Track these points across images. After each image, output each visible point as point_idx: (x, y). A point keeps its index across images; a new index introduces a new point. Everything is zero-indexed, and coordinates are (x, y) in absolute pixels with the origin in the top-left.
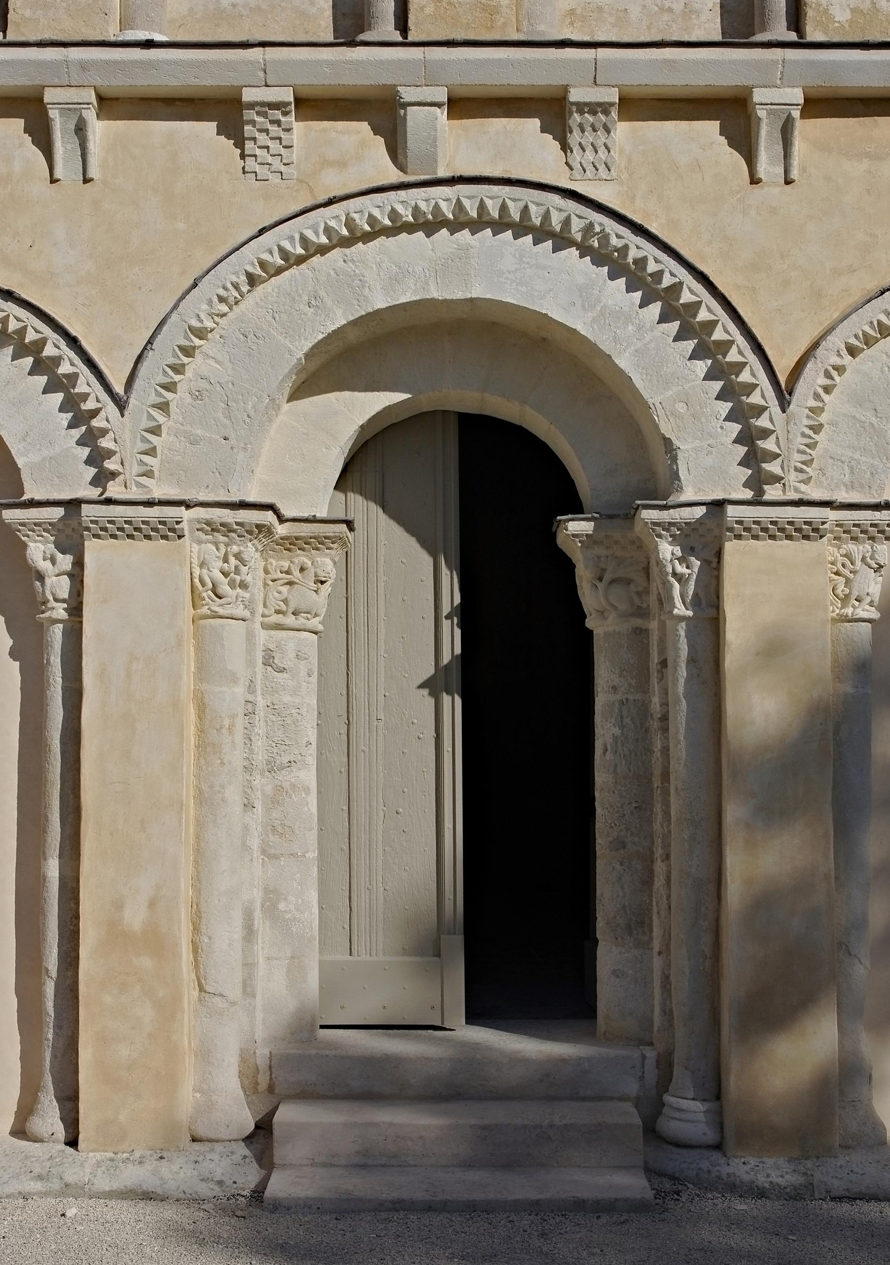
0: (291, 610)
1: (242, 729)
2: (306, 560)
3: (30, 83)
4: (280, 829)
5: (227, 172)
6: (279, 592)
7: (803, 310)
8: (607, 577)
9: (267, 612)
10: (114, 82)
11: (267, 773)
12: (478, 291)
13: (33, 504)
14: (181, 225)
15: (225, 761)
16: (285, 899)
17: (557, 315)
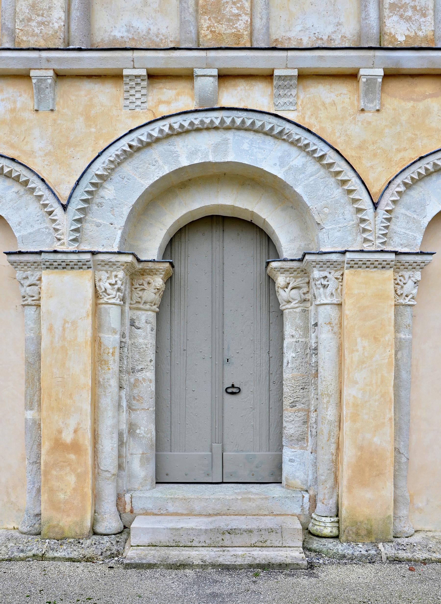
0: (143, 302)
1: (118, 354)
2: (150, 279)
3: (24, 68)
4: (137, 398)
5: (115, 106)
6: (138, 294)
7: (383, 167)
8: (290, 286)
9: (132, 302)
11: (131, 373)
12: (231, 158)
13: (285, 260)
15: (110, 368)
16: (140, 429)
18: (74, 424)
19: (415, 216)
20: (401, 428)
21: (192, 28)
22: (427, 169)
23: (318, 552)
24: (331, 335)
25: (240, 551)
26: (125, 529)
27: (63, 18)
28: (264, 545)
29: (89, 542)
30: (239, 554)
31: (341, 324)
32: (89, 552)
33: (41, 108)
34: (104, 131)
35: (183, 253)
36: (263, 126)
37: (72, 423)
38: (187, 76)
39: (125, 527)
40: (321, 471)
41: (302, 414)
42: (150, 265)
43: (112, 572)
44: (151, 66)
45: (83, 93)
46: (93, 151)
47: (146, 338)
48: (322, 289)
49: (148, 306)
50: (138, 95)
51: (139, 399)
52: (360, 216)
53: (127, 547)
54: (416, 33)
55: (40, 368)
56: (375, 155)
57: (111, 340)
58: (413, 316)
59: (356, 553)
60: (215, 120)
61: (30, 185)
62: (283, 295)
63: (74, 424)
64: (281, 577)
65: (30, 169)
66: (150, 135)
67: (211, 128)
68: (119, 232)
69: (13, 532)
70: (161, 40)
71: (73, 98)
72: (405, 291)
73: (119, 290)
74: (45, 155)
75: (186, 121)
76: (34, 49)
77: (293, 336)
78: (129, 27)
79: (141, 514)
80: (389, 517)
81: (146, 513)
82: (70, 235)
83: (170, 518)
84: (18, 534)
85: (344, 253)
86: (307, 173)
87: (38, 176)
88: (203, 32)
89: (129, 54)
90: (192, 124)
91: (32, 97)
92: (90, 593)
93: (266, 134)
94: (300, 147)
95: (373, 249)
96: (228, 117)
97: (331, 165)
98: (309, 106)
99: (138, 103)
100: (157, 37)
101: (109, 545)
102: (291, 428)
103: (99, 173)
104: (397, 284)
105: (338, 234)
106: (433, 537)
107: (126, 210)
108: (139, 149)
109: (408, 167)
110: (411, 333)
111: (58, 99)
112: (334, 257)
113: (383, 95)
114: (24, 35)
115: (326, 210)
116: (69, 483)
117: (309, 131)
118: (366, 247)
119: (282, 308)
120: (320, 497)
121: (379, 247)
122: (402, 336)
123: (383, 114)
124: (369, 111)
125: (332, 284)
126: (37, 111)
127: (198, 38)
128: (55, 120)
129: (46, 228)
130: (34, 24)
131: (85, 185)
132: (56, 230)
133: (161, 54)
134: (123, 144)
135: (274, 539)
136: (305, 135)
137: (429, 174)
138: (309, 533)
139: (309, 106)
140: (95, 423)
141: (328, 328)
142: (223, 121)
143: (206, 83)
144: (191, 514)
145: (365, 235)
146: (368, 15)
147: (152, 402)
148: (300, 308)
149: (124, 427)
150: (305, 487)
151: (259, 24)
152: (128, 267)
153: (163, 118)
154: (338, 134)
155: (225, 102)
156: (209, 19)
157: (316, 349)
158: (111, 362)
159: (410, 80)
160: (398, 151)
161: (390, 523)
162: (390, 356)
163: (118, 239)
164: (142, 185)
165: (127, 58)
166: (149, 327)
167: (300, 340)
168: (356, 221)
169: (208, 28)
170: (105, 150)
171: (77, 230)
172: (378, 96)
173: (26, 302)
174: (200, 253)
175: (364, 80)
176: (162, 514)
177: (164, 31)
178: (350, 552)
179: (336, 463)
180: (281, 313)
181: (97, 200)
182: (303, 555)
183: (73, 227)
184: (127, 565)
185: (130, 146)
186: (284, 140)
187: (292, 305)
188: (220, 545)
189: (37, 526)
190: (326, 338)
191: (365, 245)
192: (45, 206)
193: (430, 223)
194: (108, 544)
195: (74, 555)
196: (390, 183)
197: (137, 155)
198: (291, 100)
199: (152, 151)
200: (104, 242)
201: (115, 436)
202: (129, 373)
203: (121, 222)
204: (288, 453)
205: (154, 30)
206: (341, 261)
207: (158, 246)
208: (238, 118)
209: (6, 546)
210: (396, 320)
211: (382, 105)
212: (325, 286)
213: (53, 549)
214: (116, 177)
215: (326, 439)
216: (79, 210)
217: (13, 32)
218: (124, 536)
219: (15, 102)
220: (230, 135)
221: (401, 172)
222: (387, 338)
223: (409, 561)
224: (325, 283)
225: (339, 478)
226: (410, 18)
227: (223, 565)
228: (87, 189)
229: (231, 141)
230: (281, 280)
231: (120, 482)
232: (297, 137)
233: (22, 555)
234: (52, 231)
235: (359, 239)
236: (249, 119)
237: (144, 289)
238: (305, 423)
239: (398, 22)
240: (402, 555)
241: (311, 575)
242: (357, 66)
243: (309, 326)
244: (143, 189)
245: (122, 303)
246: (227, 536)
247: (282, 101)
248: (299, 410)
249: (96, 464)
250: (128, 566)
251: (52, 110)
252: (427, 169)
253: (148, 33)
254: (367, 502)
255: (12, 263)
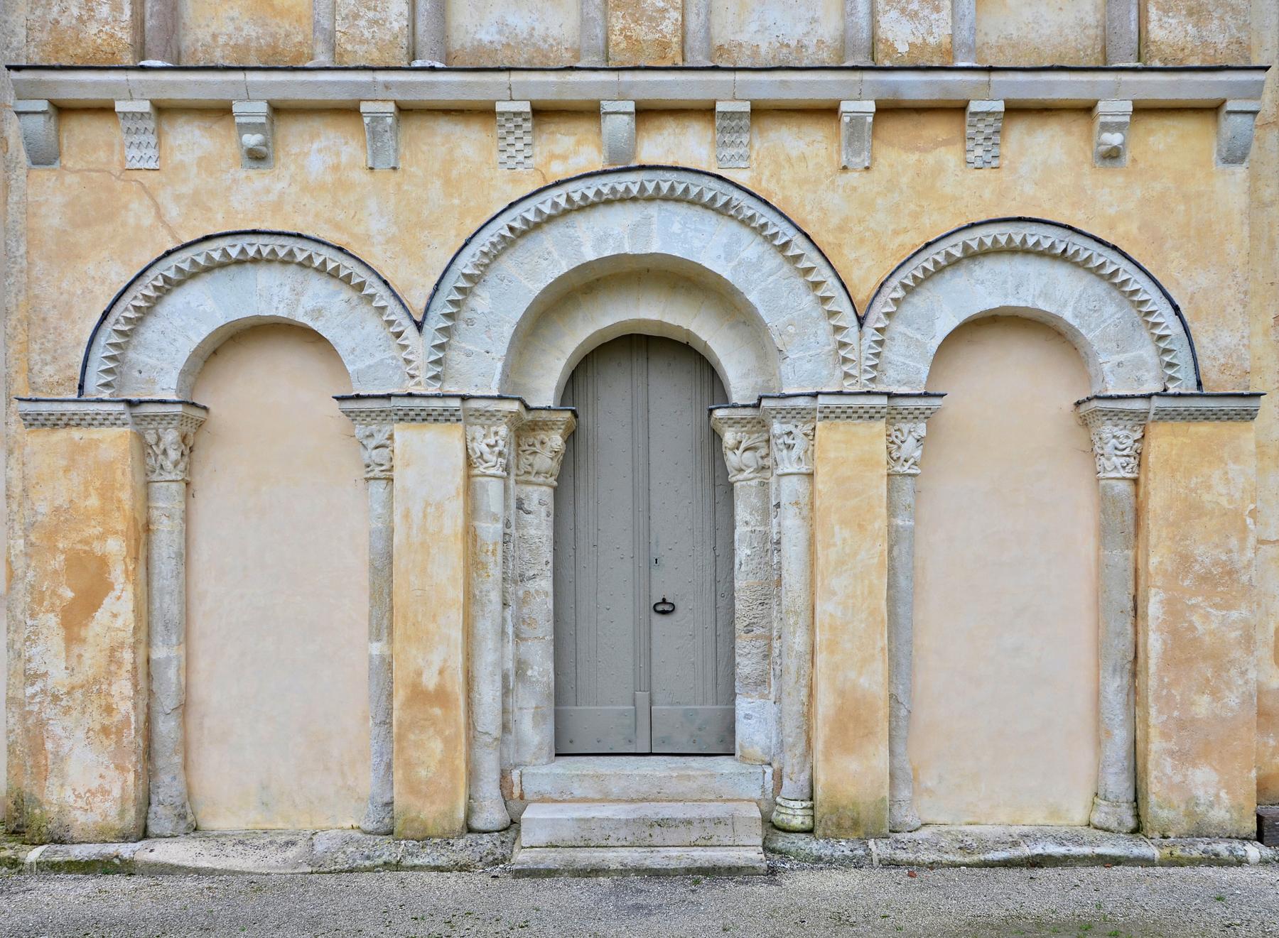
8: (742, 447)
10: (408, 98)
12: (655, 247)
13: (735, 406)
14: (456, 201)
17: (706, 265)
18: (436, 660)
19: (919, 336)
20: (899, 660)
21: (598, 30)
22: (936, 263)
23: (784, 854)
24: (798, 522)
25: (674, 852)
26: (513, 825)
27: (406, 13)
28: (709, 843)
29: (462, 842)
30: (673, 856)
31: (812, 504)
32: (463, 858)
33: (378, 165)
34: (472, 204)
35: (590, 395)
36: (700, 194)
37: (436, 659)
38: (589, 112)
39: (512, 822)
40: (787, 731)
41: (761, 642)
42: (544, 414)
43: (497, 882)
44: (538, 96)
45: (438, 140)
46: (457, 235)
47: (539, 527)
48: (785, 451)
49: (541, 479)
50: (519, 145)
51: (531, 622)
52: (838, 338)
53: (516, 850)
54: (924, 40)
55: (391, 575)
56: (862, 241)
57: (490, 530)
58: (917, 492)
59: (836, 855)
60: (631, 186)
61: (367, 291)
62: (733, 459)
63: (436, 660)
64: (730, 885)
65: (367, 265)
66: (539, 212)
67: (627, 199)
68: (499, 365)
69: (352, 832)
70: (551, 46)
71: (425, 148)
72: (904, 453)
73: (500, 454)
74: (387, 242)
75: (589, 189)
76: (365, 69)
77: (747, 523)
78: (502, 25)
79: (535, 801)
80: (883, 799)
81: (543, 799)
82: (429, 370)
83: (576, 805)
84: (358, 835)
85: (815, 395)
86: (764, 270)
87: (379, 277)
88: (614, 37)
89: (503, 77)
90: (598, 193)
91: (364, 147)
92: (469, 907)
93: (705, 206)
94: (754, 228)
95: (856, 389)
96: (650, 181)
97: (797, 258)
98: (767, 161)
99: (520, 157)
100: (545, 41)
101: (491, 844)
102: (746, 666)
103: (467, 271)
104: (892, 442)
105: (809, 366)
106: (948, 832)
107: (508, 331)
108: (523, 234)
109: (909, 259)
110: (913, 517)
111: (402, 150)
112: (801, 402)
113: (875, 143)
114: (348, 41)
115: (791, 329)
116: (433, 752)
117: (766, 203)
118: (848, 386)
119: (732, 479)
120: (787, 770)
121: (865, 386)
122: (899, 522)
123: (874, 175)
124: (855, 170)
125: (800, 443)
126: (371, 169)
127: (607, 46)
128: (399, 185)
129: (393, 358)
130: (362, 23)
131: (448, 292)
132: (408, 362)
133: (552, 77)
134: (501, 227)
135: (723, 834)
136: (762, 209)
137: (940, 269)
138: (772, 827)
139: (767, 161)
140: (468, 659)
141: (795, 510)
142: (643, 188)
143: (618, 125)
144: (606, 799)
145: (845, 368)
146: (855, 8)
147: (549, 626)
148: (756, 481)
149: (510, 665)
150: (767, 759)
151: (694, 23)
152: (514, 419)
153: (558, 184)
154: (808, 208)
155: (646, 157)
156: (623, 17)
157: (778, 543)
158: (491, 566)
159: (915, 117)
160: (896, 233)
161: (884, 809)
162: (882, 552)
163: (497, 376)
164: (530, 291)
165: (501, 83)
166: (543, 510)
167: (758, 529)
168: (834, 346)
169: (622, 30)
170: (474, 235)
171: (438, 362)
172: (867, 145)
173: (371, 475)
174: (616, 394)
175: (846, 119)
176: (564, 801)
177: (555, 31)
178: (828, 852)
179: (808, 715)
180: (731, 487)
181: (466, 314)
182: (762, 856)
183: (433, 358)
184: (518, 871)
185: (511, 229)
186: (731, 216)
187: (745, 475)
188: (647, 843)
189: (387, 820)
190: (790, 525)
191: (846, 383)
192: (390, 323)
193: (941, 347)
194: (490, 845)
195: (442, 861)
196: (882, 285)
197: (521, 242)
198: (741, 152)
199: (543, 236)
200: (478, 380)
201: (498, 678)
202: (515, 582)
203: (501, 349)
204: (743, 705)
205: (540, 30)
206: (814, 409)
207: (555, 384)
208: (666, 181)
209: (344, 852)
210: (889, 497)
211: (873, 158)
212: (789, 447)
213: (411, 854)
214: (491, 278)
215: (793, 681)
216: (439, 330)
217: (332, 33)
218: (512, 834)
219: (338, 154)
220: (654, 210)
221: (899, 267)
222: (876, 525)
223: (911, 864)
224: (790, 441)
225: (813, 740)
226: (916, 13)
227: (651, 870)
228: (450, 298)
229: (655, 220)
230: (729, 437)
231: (505, 750)
232: (749, 213)
233: (367, 863)
234: (401, 362)
235: (838, 374)
236: (680, 183)
237: (535, 453)
238: (766, 656)
239: (897, 21)
240: (901, 855)
241: (771, 883)
242: (835, 96)
243: (768, 509)
244: (532, 297)
245: (505, 474)
246: (657, 830)
247: (729, 152)
248: (757, 638)
249: (471, 725)
250: (519, 874)
251: (394, 168)
252: (936, 263)
253: (532, 35)
254: (853, 775)
255: (348, 413)
